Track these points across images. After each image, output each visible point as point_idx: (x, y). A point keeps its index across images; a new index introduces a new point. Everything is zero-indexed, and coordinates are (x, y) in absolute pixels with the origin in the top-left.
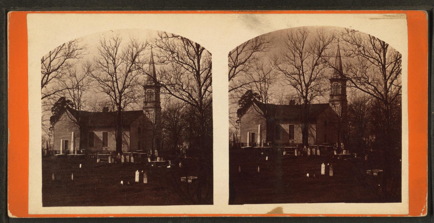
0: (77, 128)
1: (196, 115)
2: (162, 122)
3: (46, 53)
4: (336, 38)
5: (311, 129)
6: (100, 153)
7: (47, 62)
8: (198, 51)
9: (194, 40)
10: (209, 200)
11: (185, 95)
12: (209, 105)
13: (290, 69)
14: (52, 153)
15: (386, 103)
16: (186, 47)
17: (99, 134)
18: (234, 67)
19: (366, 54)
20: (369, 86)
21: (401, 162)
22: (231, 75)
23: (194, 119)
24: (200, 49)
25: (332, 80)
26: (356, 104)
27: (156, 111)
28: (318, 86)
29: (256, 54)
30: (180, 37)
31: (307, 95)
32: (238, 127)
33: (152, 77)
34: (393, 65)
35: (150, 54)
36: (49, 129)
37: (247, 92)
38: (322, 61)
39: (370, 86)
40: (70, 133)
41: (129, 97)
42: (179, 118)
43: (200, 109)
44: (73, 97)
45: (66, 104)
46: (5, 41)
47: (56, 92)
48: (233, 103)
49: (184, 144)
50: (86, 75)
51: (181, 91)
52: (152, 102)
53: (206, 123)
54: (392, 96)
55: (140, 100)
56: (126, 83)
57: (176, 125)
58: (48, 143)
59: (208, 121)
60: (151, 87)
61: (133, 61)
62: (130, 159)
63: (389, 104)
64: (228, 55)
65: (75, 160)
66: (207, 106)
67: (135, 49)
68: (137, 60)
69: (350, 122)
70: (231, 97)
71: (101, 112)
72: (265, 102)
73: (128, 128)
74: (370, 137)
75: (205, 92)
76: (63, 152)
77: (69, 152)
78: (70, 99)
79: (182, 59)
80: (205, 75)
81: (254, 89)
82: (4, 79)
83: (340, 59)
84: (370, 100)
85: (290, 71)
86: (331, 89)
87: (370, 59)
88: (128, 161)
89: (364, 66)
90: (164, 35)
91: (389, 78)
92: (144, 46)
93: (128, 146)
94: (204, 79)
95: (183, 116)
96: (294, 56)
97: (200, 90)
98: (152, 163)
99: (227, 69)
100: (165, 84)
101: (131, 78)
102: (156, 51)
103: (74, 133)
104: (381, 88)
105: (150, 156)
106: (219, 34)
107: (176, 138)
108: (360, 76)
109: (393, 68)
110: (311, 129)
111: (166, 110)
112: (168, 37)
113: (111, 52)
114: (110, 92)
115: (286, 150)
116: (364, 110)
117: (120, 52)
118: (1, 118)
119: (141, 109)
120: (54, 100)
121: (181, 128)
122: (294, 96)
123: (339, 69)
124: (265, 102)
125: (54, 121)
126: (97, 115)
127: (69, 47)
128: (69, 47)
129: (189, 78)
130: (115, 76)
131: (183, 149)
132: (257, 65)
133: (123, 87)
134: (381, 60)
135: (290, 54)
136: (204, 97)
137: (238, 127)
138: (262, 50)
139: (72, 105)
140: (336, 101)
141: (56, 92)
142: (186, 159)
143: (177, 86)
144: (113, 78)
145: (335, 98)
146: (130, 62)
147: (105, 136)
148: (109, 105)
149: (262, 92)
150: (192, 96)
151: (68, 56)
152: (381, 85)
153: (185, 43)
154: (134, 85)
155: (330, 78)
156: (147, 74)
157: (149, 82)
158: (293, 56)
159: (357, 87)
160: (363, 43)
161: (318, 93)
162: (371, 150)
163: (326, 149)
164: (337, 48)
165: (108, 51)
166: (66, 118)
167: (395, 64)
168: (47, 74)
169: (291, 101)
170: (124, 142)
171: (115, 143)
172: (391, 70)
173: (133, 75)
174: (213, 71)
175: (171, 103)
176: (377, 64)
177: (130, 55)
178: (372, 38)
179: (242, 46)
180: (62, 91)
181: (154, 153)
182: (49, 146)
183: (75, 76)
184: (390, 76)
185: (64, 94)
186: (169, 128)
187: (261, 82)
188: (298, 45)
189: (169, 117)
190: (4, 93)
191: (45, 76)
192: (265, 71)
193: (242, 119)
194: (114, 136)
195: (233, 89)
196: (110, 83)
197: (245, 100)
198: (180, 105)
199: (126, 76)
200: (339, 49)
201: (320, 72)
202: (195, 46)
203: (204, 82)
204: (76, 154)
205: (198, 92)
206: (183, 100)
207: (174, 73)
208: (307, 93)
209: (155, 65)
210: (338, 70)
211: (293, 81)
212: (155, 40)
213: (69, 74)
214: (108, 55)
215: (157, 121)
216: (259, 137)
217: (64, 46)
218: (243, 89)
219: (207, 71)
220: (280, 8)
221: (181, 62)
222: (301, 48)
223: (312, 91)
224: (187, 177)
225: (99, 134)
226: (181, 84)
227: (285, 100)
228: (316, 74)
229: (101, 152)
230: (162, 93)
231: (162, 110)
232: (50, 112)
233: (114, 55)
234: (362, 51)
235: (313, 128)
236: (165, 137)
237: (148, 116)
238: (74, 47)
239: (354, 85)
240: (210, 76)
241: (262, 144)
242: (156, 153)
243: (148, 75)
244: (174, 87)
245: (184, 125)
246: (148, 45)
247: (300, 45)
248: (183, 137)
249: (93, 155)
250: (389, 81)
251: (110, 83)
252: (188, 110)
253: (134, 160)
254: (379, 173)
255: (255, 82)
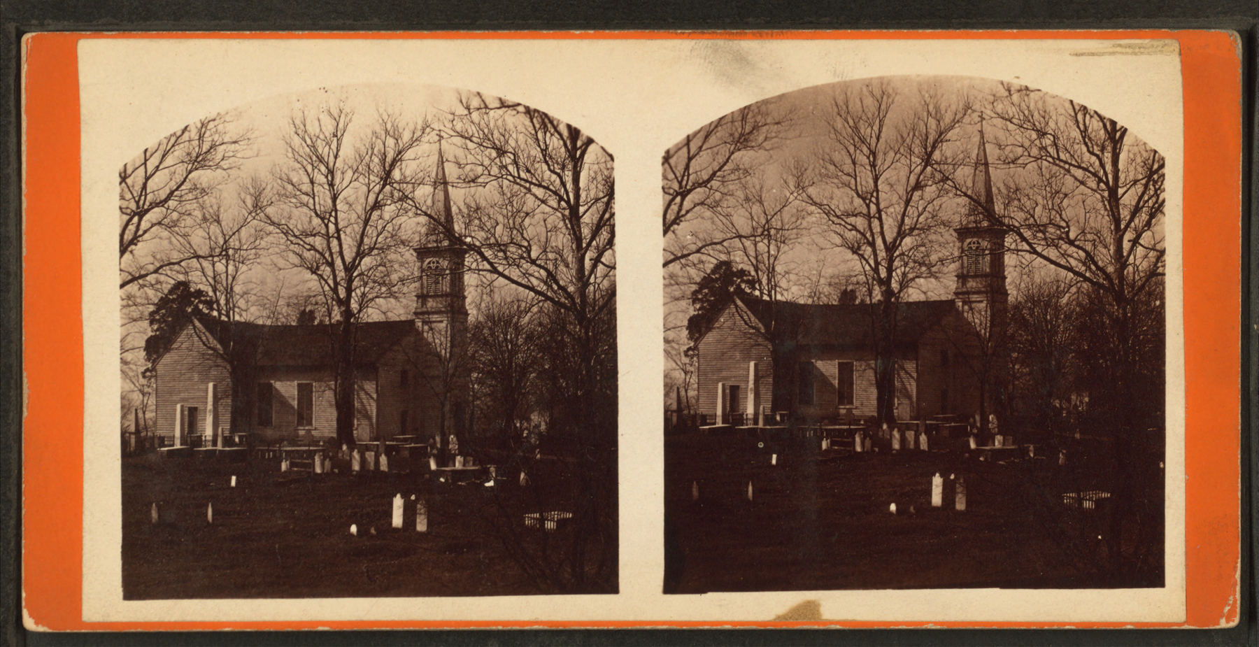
0: (223, 371)
1: (569, 334)
2: (469, 354)
3: (132, 155)
4: (974, 111)
5: (902, 374)
6: (291, 444)
7: (137, 179)
8: (575, 148)
9: (564, 115)
10: (606, 581)
11: (537, 276)
12: (605, 305)
13: (842, 199)
14: (152, 445)
15: (1120, 298)
16: (540, 135)
17: (288, 389)
18: (678, 194)
19: (1062, 156)
20: (1072, 250)
21: (1163, 470)
22: (671, 216)
23: (562, 344)
24: (579, 144)
25: (963, 233)
26: (1034, 302)
27: (452, 322)
28: (923, 249)
29: (744, 157)
30: (521, 109)
31: (890, 276)
32: (692, 369)
33: (440, 224)
34: (1139, 188)
35: (435, 158)
36: (144, 374)
37: (717, 268)
38: (933, 176)
39: (1075, 249)
40: (202, 387)
41: (374, 282)
42: (520, 341)
43: (581, 317)
44: (211, 281)
45: (191, 303)
46: (13, 119)
47: (161, 267)
48: (677, 299)
49: (535, 417)
50: (250, 218)
51: (526, 265)
52: (442, 296)
53: (1137, 337)
54: (1137, 278)
55: (405, 289)
56: (366, 240)
57: (511, 363)
58: (141, 415)
59: (604, 352)
60: (437, 252)
61: (386, 178)
62: (377, 462)
63: (1128, 302)
64: (660, 160)
65: (218, 464)
66: (601, 309)
67: (390, 142)
68: (396, 174)
69: (1015, 355)
70: (671, 281)
71: (294, 324)
72: (770, 296)
73: (370, 370)
74: (1073, 397)
75: (594, 266)
76: (183, 441)
77: (199, 441)
78: (202, 287)
79: (528, 171)
80: (596, 218)
81: (738, 259)
82: (12, 229)
83: (987, 173)
84: (1074, 290)
85: (841, 207)
86: (960, 257)
87: (1073, 170)
88: (372, 467)
89: (1057, 192)
90: (475, 103)
91: (1128, 226)
92: (419, 133)
93: (371, 424)
94: (592, 229)
95: (530, 338)
96: (854, 163)
97: (581, 261)
98: (442, 473)
99: (659, 202)
100: (478, 244)
101: (380, 228)
102: (453, 147)
103: (215, 387)
104: (1104, 256)
105: (435, 451)
106: (635, 99)
107: (510, 401)
108: (1045, 220)
109: (1141, 198)
110: (902, 374)
111: (481, 319)
112: (486, 107)
113: (323, 150)
114: (318, 268)
115: (830, 434)
116: (1057, 318)
117: (347, 151)
118: (3, 343)
119: (410, 317)
120: (157, 290)
121: (524, 370)
122: (854, 280)
123: (983, 199)
124: (770, 296)
125: (157, 352)
126: (280, 333)
127: (201, 137)
128: (201, 137)
129: (549, 226)
130: (332, 219)
131: (530, 433)
132: (745, 187)
133: (358, 254)
134: (1106, 173)
135: (840, 156)
136: (592, 280)
137: (689, 368)
138: (218, 166)
139: (209, 304)
140: (433, 313)
141: (161, 267)
142: (541, 460)
143: (512, 249)
144: (327, 226)
145: (972, 284)
146: (377, 180)
147: (305, 394)
148: (317, 303)
149: (761, 266)
150: (558, 277)
151: (198, 161)
152: (1106, 247)
153: (537, 126)
154: (389, 247)
155: (415, 245)
156: (426, 214)
157: (434, 238)
158: (849, 161)
159: (1034, 252)
160: (1052, 124)
161: (924, 269)
162: (1077, 436)
163: (945, 433)
164: (976, 139)
165: (313, 147)
166: (191, 342)
167: (1146, 186)
168: (135, 214)
169: (844, 293)
170: (359, 412)
171: (333, 414)
172: (1134, 203)
173: (387, 216)
174: (619, 205)
175: (1037, 280)
176: (1094, 185)
177: (376, 160)
178: (1080, 112)
179: (702, 134)
180: (178, 263)
181: (448, 443)
182: (142, 422)
183: (218, 222)
184: (1131, 220)
185: (186, 273)
186: (489, 372)
187: (758, 239)
188: (865, 130)
189: (490, 339)
190: (13, 268)
191: (130, 220)
192: (770, 205)
193: (701, 346)
194: (329, 395)
195: (676, 258)
196: (319, 242)
197: (711, 289)
198: (523, 305)
199: (366, 222)
200: (983, 144)
201: (930, 208)
202: (565, 133)
203: (593, 239)
204: (219, 447)
205: (574, 266)
206: (532, 289)
207: (505, 212)
208: (890, 270)
209: (450, 188)
210: (980, 204)
211: (851, 235)
212: (451, 117)
213: (743, 197)
214: (314, 158)
215: (456, 350)
216: (751, 397)
217: (186, 134)
218: (704, 258)
219: (600, 206)
220: (811, 22)
221: (526, 181)
222: (874, 140)
223: (906, 264)
224: (541, 515)
225: (288, 389)
226: (526, 244)
227: (827, 290)
228: (916, 214)
229: (294, 440)
230: (470, 269)
231: (471, 319)
232: (146, 324)
233: (332, 159)
234: (1049, 149)
235: (907, 373)
236: (479, 398)
237: (428, 336)
238: (216, 137)
239: (1028, 248)
240: (609, 219)
241: (761, 418)
242: (453, 445)
243: (430, 216)
244: (505, 253)
245: (533, 362)
246: (428, 130)
247: (869, 130)
248: (532, 398)
249: (269, 451)
250: (1129, 236)
251: (319, 242)
252: (546, 320)
253: (389, 465)
254: (1099, 503)
255: (740, 237)
